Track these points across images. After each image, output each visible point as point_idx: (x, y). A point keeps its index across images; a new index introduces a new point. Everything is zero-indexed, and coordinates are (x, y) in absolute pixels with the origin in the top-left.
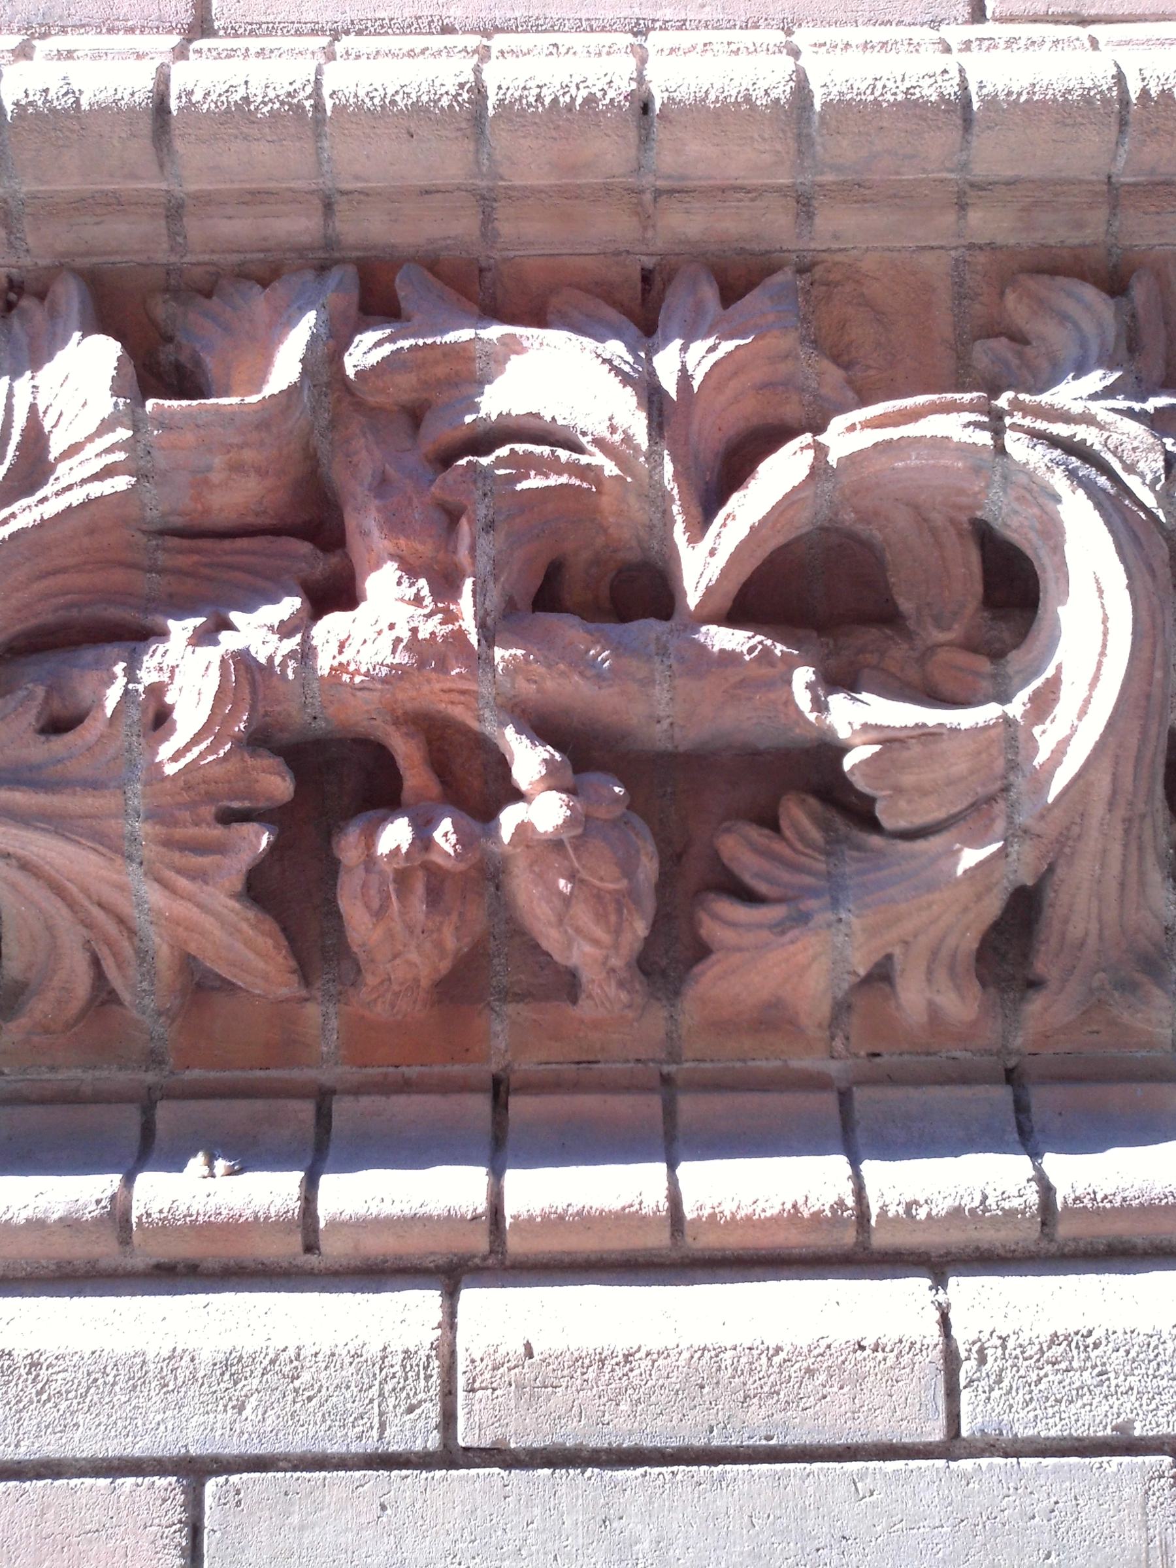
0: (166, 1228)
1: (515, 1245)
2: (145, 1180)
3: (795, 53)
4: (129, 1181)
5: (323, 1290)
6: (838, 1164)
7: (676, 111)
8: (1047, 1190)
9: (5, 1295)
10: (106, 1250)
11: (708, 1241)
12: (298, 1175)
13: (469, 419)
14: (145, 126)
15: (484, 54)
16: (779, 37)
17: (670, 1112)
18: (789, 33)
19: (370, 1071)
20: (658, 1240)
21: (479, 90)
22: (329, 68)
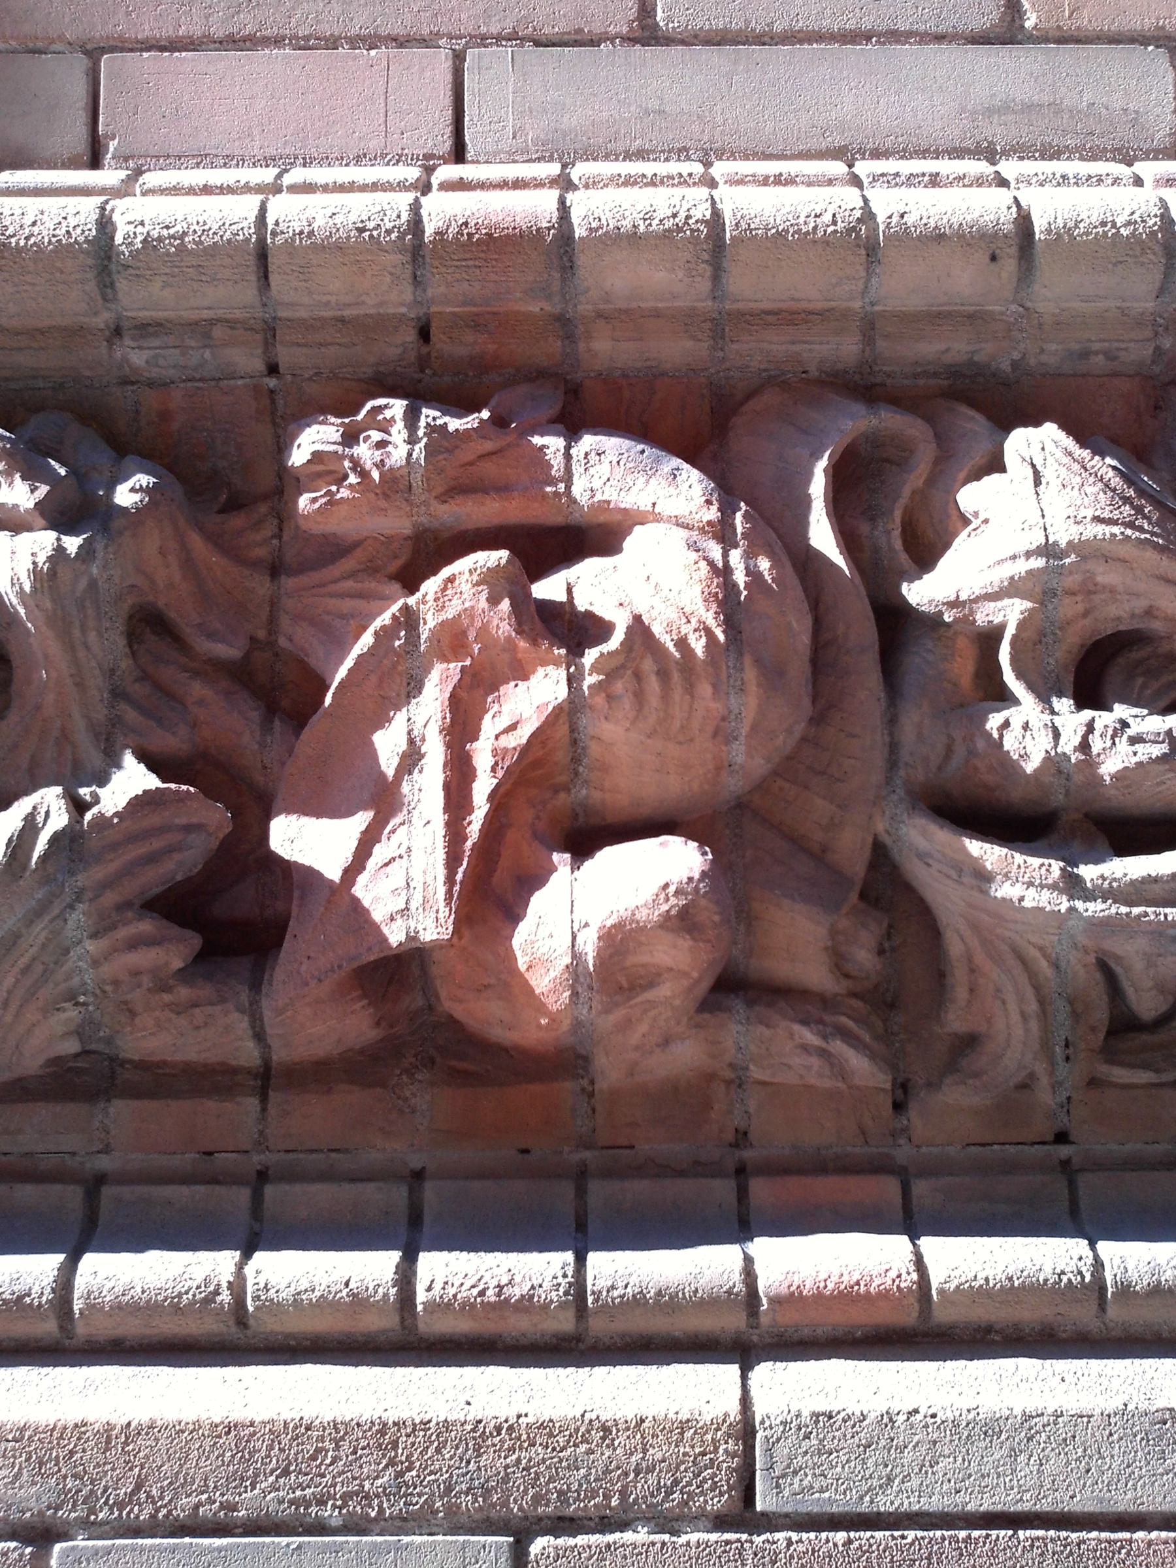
0: (790, 1300)
1: (81, 1330)
2: (261, 1258)
3: (712, 184)
4: (581, 1260)
5: (818, 1358)
6: (901, 1242)
7: (748, 238)
8: (1098, 1264)
9: (3, 1369)
10: (1084, 1316)
11: (273, 1326)
12: (395, 1256)
13: (72, 544)
14: (251, 261)
15: (564, 183)
16: (697, 168)
17: (742, 1193)
18: (707, 165)
19: (932, 1149)
20: (909, 1317)
21: (416, 224)
22: (424, 200)
